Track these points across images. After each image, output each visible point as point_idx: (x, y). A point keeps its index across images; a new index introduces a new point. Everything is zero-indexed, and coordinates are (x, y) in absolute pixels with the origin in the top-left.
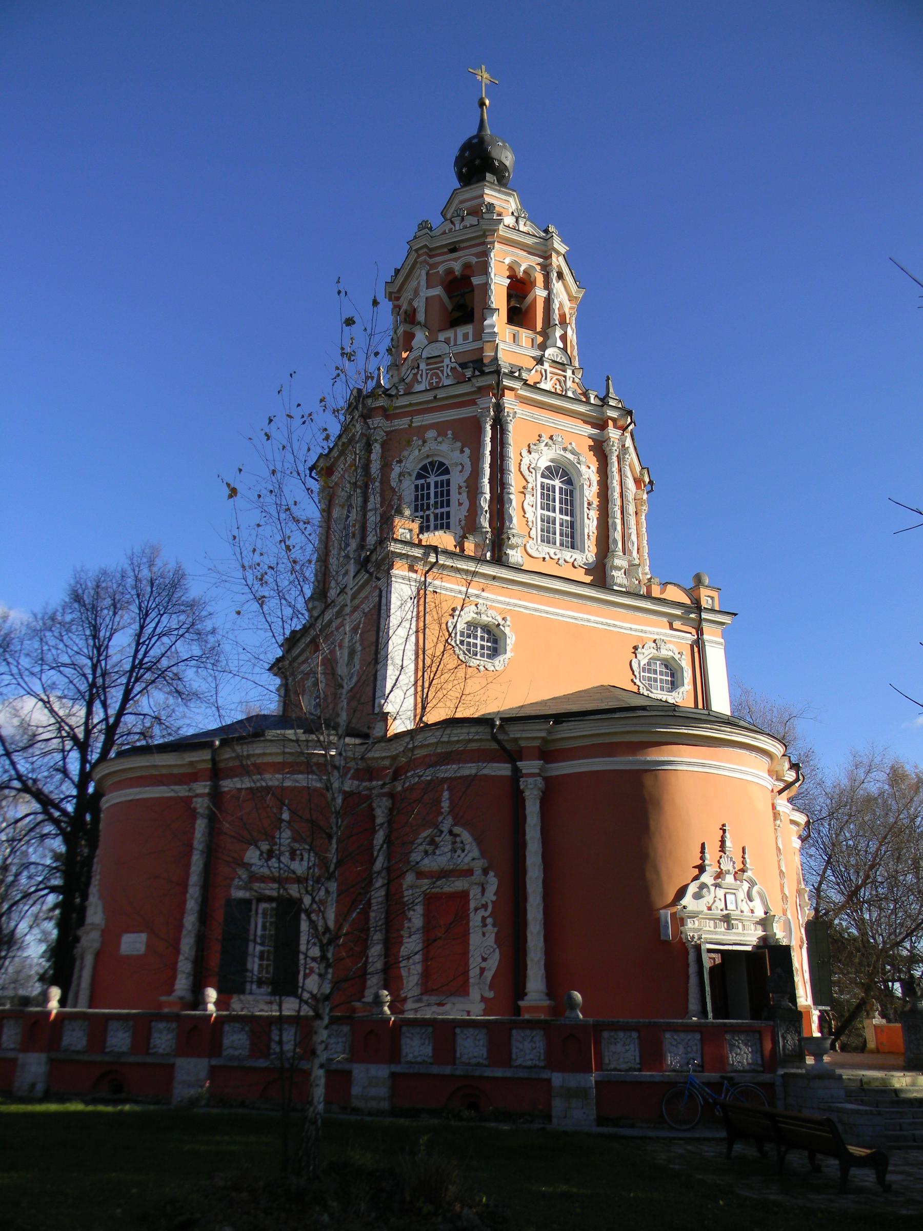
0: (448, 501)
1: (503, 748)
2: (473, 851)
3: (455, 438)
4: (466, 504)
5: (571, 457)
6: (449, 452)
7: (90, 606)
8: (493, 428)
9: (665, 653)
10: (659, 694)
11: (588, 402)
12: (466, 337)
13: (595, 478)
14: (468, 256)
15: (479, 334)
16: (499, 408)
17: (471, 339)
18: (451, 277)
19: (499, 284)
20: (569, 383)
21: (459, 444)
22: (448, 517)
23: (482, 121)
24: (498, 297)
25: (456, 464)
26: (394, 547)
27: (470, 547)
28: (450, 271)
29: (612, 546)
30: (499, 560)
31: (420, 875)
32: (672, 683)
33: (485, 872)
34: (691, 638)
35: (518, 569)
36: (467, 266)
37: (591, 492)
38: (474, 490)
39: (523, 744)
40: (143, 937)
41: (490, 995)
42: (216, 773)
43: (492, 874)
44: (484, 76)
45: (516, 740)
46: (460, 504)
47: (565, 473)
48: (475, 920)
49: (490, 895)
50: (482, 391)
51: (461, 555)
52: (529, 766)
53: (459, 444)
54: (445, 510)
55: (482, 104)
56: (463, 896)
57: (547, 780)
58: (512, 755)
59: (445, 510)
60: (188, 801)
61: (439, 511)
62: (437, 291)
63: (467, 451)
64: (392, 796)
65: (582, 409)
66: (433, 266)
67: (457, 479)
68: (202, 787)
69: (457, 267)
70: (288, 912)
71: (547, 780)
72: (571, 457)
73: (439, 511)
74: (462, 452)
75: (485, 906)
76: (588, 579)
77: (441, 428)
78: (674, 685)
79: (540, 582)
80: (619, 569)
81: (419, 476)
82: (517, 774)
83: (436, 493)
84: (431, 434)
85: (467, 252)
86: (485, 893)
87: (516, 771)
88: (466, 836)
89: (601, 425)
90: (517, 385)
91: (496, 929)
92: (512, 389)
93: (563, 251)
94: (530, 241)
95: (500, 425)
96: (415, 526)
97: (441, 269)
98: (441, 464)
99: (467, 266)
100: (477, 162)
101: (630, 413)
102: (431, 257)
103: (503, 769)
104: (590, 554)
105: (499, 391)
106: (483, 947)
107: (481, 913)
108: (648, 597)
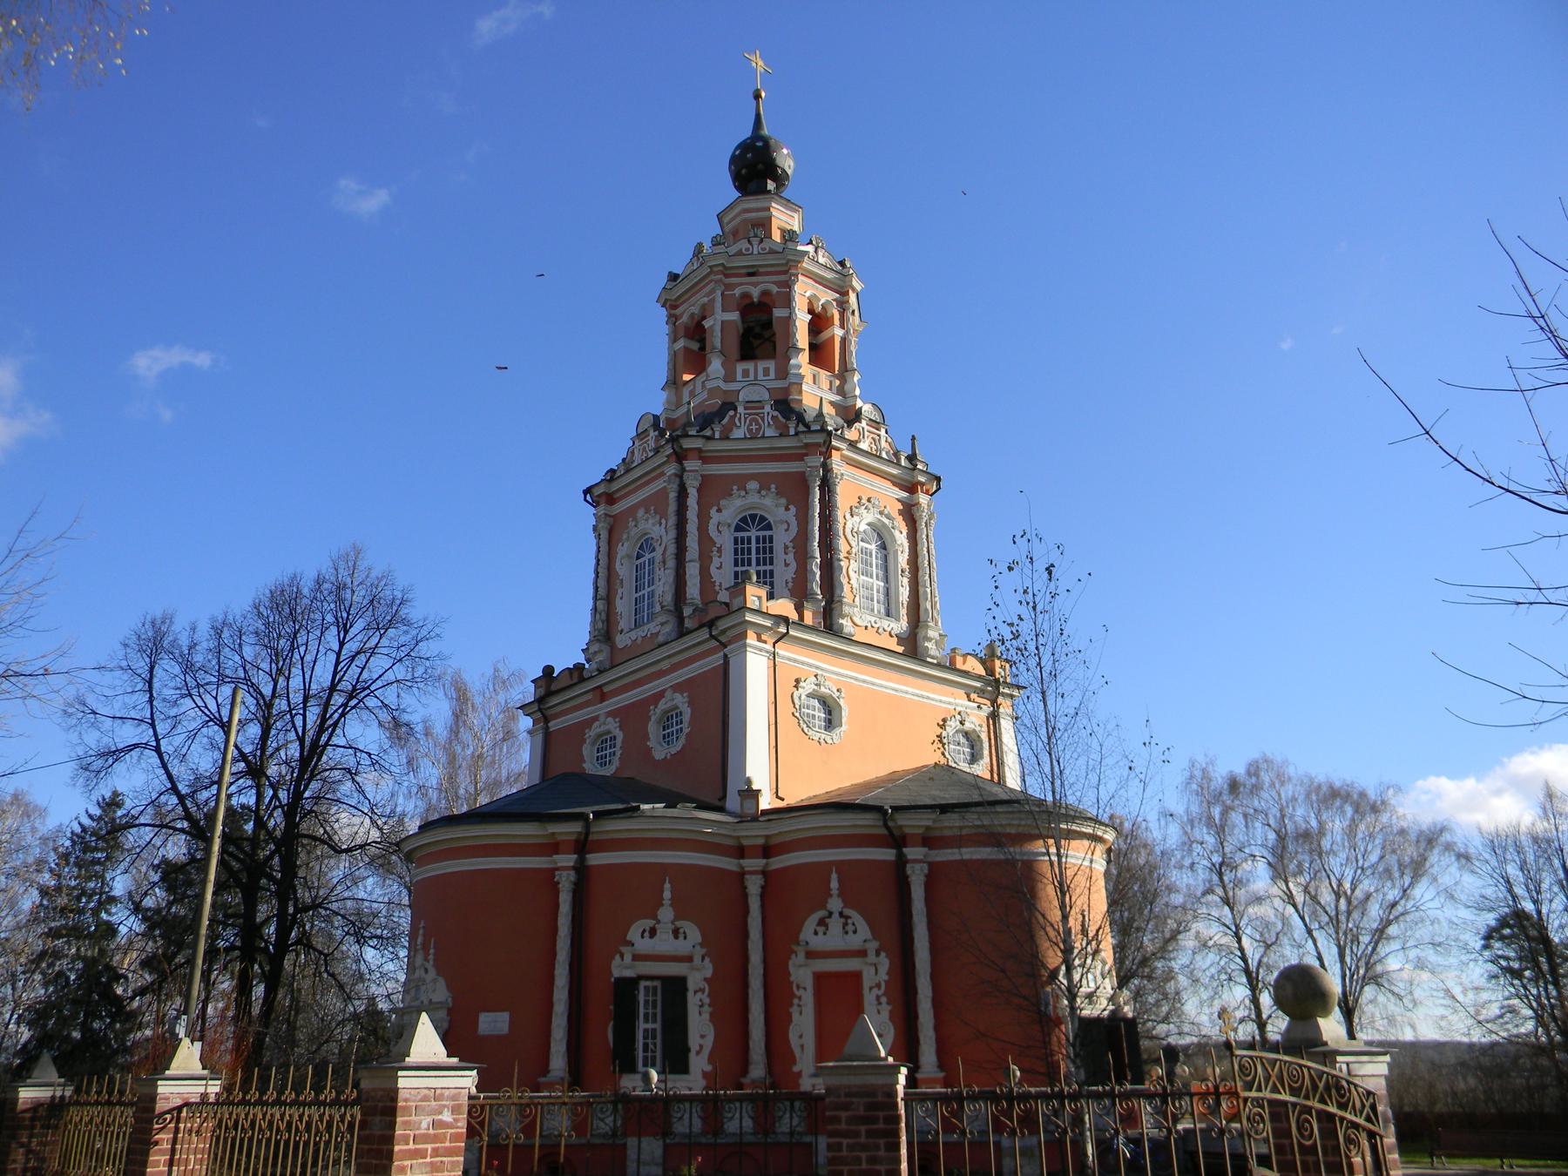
0: (771, 559)
1: (891, 834)
2: (864, 931)
3: (779, 494)
4: (794, 565)
5: (886, 521)
6: (773, 507)
7: (286, 616)
8: (821, 488)
9: (968, 726)
10: (964, 766)
11: (898, 464)
12: (766, 372)
13: (906, 545)
14: (769, 284)
15: (783, 372)
16: (827, 469)
17: (772, 375)
18: (747, 301)
19: (802, 319)
20: (883, 444)
21: (783, 501)
22: (736, 561)
23: (758, 116)
24: (802, 338)
25: (782, 522)
26: (749, 617)
27: (809, 618)
28: (746, 295)
29: (922, 618)
30: (829, 623)
31: (811, 955)
32: (972, 755)
33: (878, 953)
34: (987, 709)
35: (849, 640)
36: (765, 293)
37: (903, 559)
38: (803, 557)
39: (907, 831)
40: (505, 1016)
41: (709, 1068)
42: (582, 846)
43: (883, 954)
44: (759, 64)
45: (901, 827)
46: (787, 565)
47: (753, 517)
48: (869, 998)
49: (883, 976)
50: (810, 449)
51: (800, 624)
52: (912, 852)
53: (783, 501)
54: (768, 568)
55: (757, 96)
56: (857, 976)
57: (931, 865)
58: (898, 841)
59: (768, 568)
60: (552, 872)
61: (762, 568)
62: (734, 316)
63: (793, 509)
64: (764, 873)
65: (895, 471)
66: (728, 287)
67: (782, 538)
68: (567, 860)
69: (755, 293)
70: (675, 989)
71: (931, 865)
72: (886, 521)
73: (762, 568)
74: (787, 509)
75: (878, 986)
76: (900, 649)
77: (764, 481)
78: (974, 758)
79: (868, 652)
80: (930, 640)
81: (738, 529)
82: (901, 863)
83: (758, 549)
84: (753, 485)
85: (767, 278)
86: (876, 973)
87: (900, 855)
88: (856, 917)
89: (912, 488)
90: (843, 446)
91: (796, 1069)
92: (838, 449)
93: (858, 288)
94: (829, 275)
95: (827, 486)
96: (763, 593)
97: (737, 292)
98: (763, 519)
99: (765, 293)
100: (760, 166)
101: (938, 479)
102: (727, 276)
103: (888, 854)
104: (901, 625)
105: (828, 450)
106: (700, 1029)
107: (875, 991)
108: (952, 668)
